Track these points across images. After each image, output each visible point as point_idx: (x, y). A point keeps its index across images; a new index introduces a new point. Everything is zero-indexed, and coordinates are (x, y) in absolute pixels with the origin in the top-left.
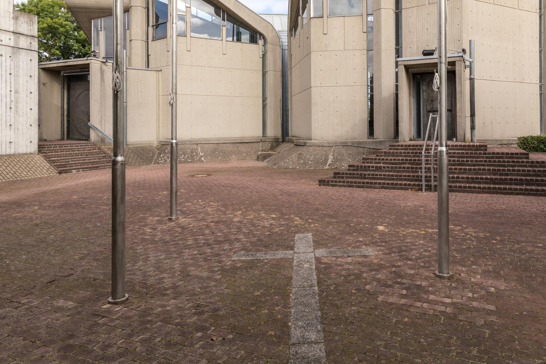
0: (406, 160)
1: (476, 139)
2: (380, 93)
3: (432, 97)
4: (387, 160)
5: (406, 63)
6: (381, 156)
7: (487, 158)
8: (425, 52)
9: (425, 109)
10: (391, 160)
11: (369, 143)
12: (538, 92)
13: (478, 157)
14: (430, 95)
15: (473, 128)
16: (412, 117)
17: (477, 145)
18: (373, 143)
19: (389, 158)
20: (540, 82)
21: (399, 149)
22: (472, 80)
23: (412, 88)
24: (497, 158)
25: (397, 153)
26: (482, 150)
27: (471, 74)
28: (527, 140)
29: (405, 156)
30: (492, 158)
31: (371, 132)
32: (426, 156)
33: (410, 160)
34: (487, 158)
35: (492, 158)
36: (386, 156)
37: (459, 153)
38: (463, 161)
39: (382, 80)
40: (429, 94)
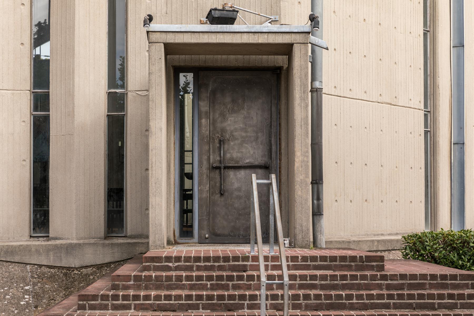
0: (199, 297)
1: (323, 239)
2: (71, 114)
3: (223, 130)
4: (147, 297)
5: (171, 39)
6: (126, 288)
7: (389, 287)
8: (216, 14)
9: (205, 163)
10: (158, 298)
11: (38, 252)
12: (422, 129)
13: (368, 287)
14: (219, 125)
15: (317, 212)
16: (172, 180)
17: (361, 257)
18: (48, 250)
19: (153, 293)
20: (426, 106)
21: (168, 269)
22: (316, 93)
23: (172, 106)
24: (411, 287)
25: (169, 278)
26: (372, 268)
27: (313, 80)
28: (422, 243)
29: (192, 287)
30: (401, 287)
31: (41, 219)
32: (269, 287)
33: (210, 298)
34: (389, 287)
35: (401, 287)
36: (139, 288)
37: (324, 278)
38: (339, 297)
39: (76, 79)
40: (214, 123)
